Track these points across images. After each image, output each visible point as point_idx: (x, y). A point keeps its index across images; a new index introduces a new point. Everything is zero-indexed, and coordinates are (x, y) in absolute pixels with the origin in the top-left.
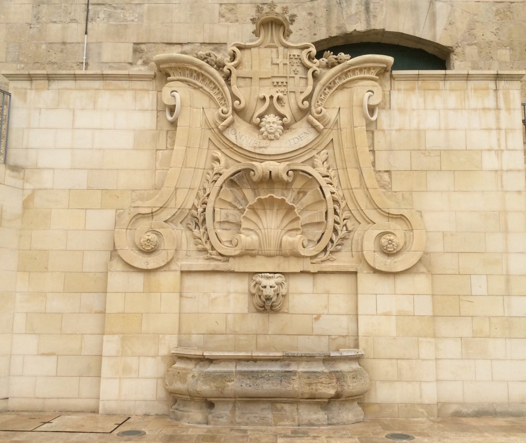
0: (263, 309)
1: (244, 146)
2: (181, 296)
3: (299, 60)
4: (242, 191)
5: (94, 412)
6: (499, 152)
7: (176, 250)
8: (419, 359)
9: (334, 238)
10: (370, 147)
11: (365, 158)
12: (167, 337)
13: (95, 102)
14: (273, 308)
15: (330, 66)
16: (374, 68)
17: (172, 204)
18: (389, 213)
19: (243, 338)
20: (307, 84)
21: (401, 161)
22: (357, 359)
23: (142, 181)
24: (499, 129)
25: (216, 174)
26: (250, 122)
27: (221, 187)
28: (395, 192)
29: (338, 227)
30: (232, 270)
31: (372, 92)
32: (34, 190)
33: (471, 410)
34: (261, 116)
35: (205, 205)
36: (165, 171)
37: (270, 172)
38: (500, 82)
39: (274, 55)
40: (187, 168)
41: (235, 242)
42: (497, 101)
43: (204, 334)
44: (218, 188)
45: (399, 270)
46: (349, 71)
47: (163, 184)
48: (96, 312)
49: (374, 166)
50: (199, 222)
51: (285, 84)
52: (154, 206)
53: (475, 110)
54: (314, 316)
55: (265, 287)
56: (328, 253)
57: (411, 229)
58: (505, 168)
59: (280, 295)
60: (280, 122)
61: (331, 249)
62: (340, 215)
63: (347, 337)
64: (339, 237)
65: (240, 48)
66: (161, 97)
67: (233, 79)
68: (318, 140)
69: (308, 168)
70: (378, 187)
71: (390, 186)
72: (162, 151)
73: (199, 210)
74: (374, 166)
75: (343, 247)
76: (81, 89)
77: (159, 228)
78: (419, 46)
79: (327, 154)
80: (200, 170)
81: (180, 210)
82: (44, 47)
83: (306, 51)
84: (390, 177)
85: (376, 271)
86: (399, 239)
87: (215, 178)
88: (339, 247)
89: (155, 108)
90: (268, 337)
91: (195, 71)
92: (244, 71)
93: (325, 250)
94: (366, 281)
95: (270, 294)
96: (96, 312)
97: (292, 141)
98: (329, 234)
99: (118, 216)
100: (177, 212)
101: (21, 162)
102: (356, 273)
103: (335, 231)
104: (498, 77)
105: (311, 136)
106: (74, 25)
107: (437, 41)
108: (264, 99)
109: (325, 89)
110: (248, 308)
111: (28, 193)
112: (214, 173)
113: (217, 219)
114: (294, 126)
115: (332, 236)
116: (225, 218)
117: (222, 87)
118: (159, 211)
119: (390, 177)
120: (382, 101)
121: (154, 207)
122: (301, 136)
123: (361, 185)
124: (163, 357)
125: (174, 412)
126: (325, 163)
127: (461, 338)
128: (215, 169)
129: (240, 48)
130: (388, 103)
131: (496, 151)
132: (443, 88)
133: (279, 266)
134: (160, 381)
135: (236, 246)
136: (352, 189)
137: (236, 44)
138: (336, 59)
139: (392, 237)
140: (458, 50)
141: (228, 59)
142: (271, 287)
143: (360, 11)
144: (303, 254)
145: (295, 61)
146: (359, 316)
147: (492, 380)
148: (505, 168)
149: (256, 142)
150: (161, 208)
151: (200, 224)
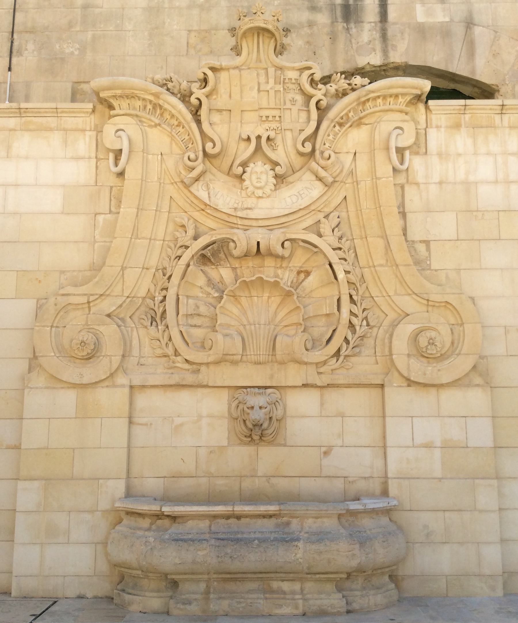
0: (250, 439)
1: (220, 207)
2: (130, 422)
3: (297, 86)
4: (219, 271)
5: (5, 593)
7: (123, 356)
9: (350, 338)
10: (399, 207)
11: (393, 224)
12: (110, 483)
13: (9, 148)
14: (263, 438)
15: (340, 95)
17: (117, 290)
18: (428, 300)
20: (309, 120)
21: (445, 226)
22: (387, 511)
23: (76, 258)
25: (181, 247)
26: (229, 172)
27: (188, 265)
28: (436, 270)
29: (355, 321)
30: (205, 383)
31: (401, 128)
34: (244, 164)
35: (165, 291)
36: (108, 244)
37: (258, 243)
39: (262, 79)
40: (139, 239)
41: (208, 344)
43: (165, 477)
44: (184, 267)
45: (444, 381)
46: (368, 100)
47: (104, 263)
48: (8, 448)
49: (405, 234)
50: (157, 318)
51: (277, 118)
52: (91, 293)
54: (323, 449)
55: (252, 408)
56: (341, 359)
57: (460, 322)
59: (274, 419)
60: (272, 172)
61: (346, 353)
62: (359, 305)
63: (371, 480)
64: (357, 336)
65: (213, 69)
66: (102, 141)
67: (203, 112)
68: (325, 198)
69: (313, 238)
70: (412, 264)
71: (428, 263)
72: (103, 216)
73: (156, 299)
74: (405, 234)
75: (363, 349)
77: (99, 325)
79: (338, 217)
80: (158, 242)
81: (130, 299)
83: (307, 73)
84: (428, 249)
85: (410, 383)
86: (444, 337)
87: (179, 253)
88: (357, 350)
89: (93, 155)
90: (257, 480)
91: (151, 102)
92: (221, 101)
93: (338, 353)
94: (398, 397)
95: (258, 418)
96: (8, 448)
97: (288, 200)
98: (343, 331)
99: (39, 308)
100: (125, 301)
103: (351, 325)
105: (317, 189)
107: (478, 78)
108: (249, 139)
109: (335, 126)
110: (228, 438)
112: (178, 245)
114: (290, 179)
115: (347, 334)
116: (194, 310)
117: (188, 123)
119: (428, 249)
120: (415, 143)
122: (301, 192)
123: (387, 261)
124: (104, 512)
125: (119, 594)
126: (336, 230)
128: (179, 240)
129: (213, 69)
130: (423, 145)
132: (500, 125)
133: (271, 377)
134: (100, 547)
135: (210, 349)
136: (374, 267)
137: (208, 64)
138: (349, 84)
139: (433, 334)
141: (197, 85)
142: (261, 408)
143: (374, 39)
144: (306, 360)
145: (291, 86)
146: (388, 449)
149: (237, 202)
150: (101, 295)
151: (158, 319)
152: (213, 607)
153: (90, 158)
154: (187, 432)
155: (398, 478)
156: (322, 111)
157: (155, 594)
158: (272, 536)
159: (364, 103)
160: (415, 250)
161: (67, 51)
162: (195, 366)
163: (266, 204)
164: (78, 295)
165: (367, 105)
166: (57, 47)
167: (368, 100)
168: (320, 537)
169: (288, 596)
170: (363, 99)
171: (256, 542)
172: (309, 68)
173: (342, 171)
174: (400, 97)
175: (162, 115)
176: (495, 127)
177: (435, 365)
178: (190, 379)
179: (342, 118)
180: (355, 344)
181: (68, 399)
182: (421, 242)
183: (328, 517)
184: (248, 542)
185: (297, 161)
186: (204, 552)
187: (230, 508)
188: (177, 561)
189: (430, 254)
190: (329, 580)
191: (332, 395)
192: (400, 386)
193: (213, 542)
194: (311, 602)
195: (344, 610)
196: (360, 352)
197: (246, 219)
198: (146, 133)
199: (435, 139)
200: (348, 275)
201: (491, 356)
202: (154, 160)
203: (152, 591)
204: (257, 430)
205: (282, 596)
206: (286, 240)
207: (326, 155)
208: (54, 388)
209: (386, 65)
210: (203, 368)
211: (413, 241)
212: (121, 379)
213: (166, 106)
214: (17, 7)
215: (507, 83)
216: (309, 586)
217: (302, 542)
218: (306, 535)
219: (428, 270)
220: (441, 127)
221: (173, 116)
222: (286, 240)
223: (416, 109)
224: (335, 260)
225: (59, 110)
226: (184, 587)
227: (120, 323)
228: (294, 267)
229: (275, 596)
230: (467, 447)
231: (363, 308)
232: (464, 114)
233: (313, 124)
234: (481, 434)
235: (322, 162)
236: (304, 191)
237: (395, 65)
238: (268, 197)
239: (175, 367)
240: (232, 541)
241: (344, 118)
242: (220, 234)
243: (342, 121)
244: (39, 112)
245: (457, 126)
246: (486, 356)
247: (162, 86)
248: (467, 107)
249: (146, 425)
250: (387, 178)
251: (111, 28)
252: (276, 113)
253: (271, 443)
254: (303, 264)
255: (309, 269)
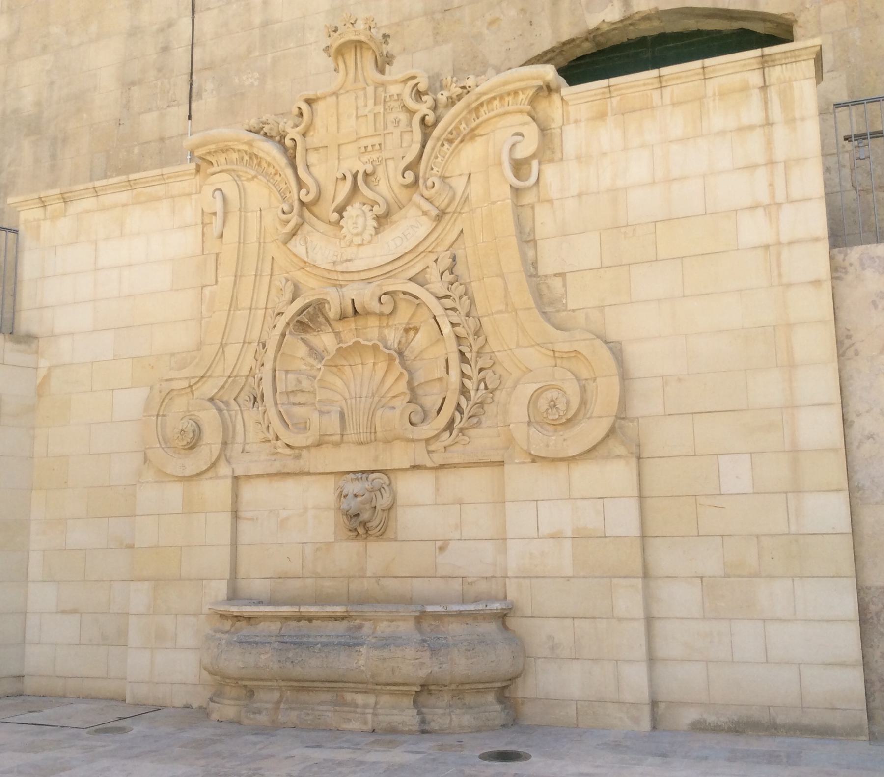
6: (772, 208)
8: (613, 617)
12: (214, 583)
16: (523, 90)
19: (310, 580)
24: (771, 163)
28: (573, 311)
31: (520, 134)
32: (49, 368)
33: (723, 719)
37: (353, 300)
38: (771, 68)
39: (361, 103)
42: (766, 109)
46: (482, 104)
51: (377, 147)
53: (722, 133)
54: (439, 544)
56: (455, 432)
58: (784, 239)
59: (378, 508)
60: (370, 213)
61: (461, 425)
62: (473, 364)
64: (471, 403)
68: (435, 235)
71: (564, 301)
72: (209, 288)
76: (103, 209)
77: (199, 411)
78: (736, 25)
81: (231, 379)
82: (136, 150)
88: (475, 420)
89: (200, 221)
91: (246, 152)
92: (314, 139)
94: (521, 478)
100: (226, 382)
101: (34, 329)
102: (501, 463)
103: (464, 391)
104: (766, 62)
106: (174, 110)
109: (443, 145)
110: (335, 533)
111: (42, 373)
113: (280, 387)
115: (459, 399)
118: (200, 384)
121: (193, 378)
123: (507, 305)
127: (702, 578)
131: (766, 207)
133: (376, 459)
139: (554, 394)
140: (801, 20)
142: (356, 496)
147: (767, 662)
148: (784, 239)
150: (202, 377)
152: (281, 718)
153: (196, 225)
154: (291, 526)
155: (517, 577)
156: (426, 127)
157: (232, 702)
158: (336, 641)
159: (477, 109)
160: (548, 287)
161: (247, 83)
162: (297, 451)
163: (355, 253)
164: (180, 379)
165: (482, 111)
166: (236, 80)
167: (482, 104)
168: (387, 642)
169: (359, 710)
170: (474, 105)
171: (319, 646)
172: (414, 77)
173: (453, 199)
174: (520, 93)
175: (259, 164)
176: (653, 108)
177: (561, 433)
178: (292, 466)
179: (451, 133)
180: (470, 414)
181: (174, 492)
182: (555, 275)
183: (405, 620)
184: (309, 646)
185: (403, 194)
186: (267, 656)
187: (296, 609)
188: (241, 664)
189: (566, 291)
190: (404, 694)
191: (449, 478)
192: (523, 463)
193: (276, 645)
194: (381, 718)
195: (416, 728)
196: (479, 423)
197: (347, 273)
198: (244, 190)
199: (572, 139)
200: (456, 329)
201: (642, 417)
202: (253, 218)
203: (231, 699)
204: (364, 521)
205: (352, 709)
206: (384, 294)
207: (429, 183)
208: (162, 482)
209: (629, 18)
210: (304, 452)
211: (546, 276)
212: (224, 470)
213: (261, 154)
214: (195, 41)
215: (808, 6)
216: (385, 699)
217: (365, 647)
218: (374, 640)
219: (564, 311)
220: (580, 121)
221: (269, 165)
222: (384, 294)
223: (550, 102)
224: (438, 311)
225: (165, 177)
226: (261, 695)
227: (222, 406)
228: (400, 324)
229: (346, 709)
230: (605, 537)
231: (478, 367)
232: (611, 97)
233: (417, 147)
234: (624, 520)
235: (426, 193)
236: (411, 228)
237: (641, 15)
238: (370, 242)
239: (277, 453)
240: (295, 645)
241: (454, 132)
242: (313, 295)
243: (451, 137)
244: (148, 182)
245: (602, 116)
246: (638, 418)
247: (257, 132)
248: (612, 89)
249: (252, 519)
250: (503, 200)
251: (292, 45)
252: (376, 140)
253: (381, 536)
254: (410, 319)
255: (417, 325)
